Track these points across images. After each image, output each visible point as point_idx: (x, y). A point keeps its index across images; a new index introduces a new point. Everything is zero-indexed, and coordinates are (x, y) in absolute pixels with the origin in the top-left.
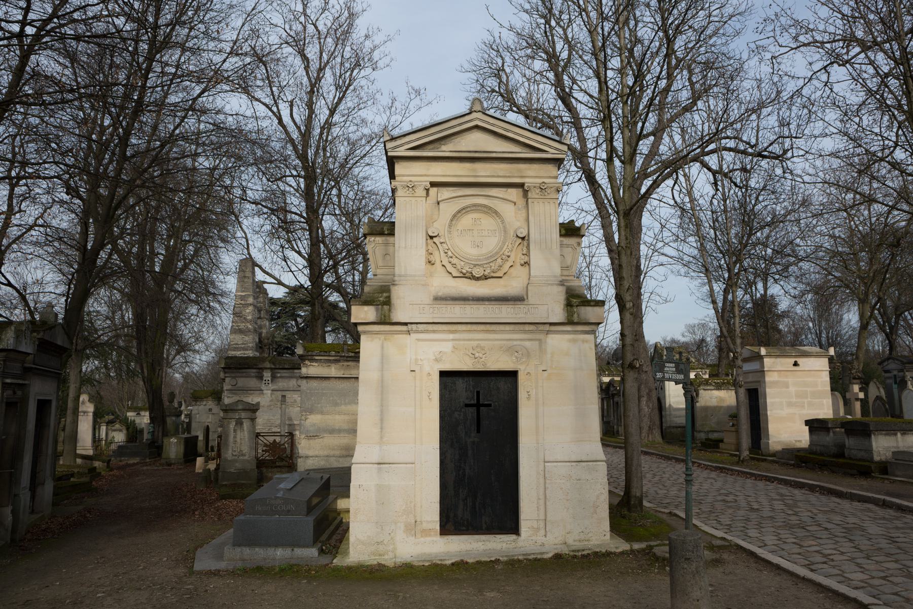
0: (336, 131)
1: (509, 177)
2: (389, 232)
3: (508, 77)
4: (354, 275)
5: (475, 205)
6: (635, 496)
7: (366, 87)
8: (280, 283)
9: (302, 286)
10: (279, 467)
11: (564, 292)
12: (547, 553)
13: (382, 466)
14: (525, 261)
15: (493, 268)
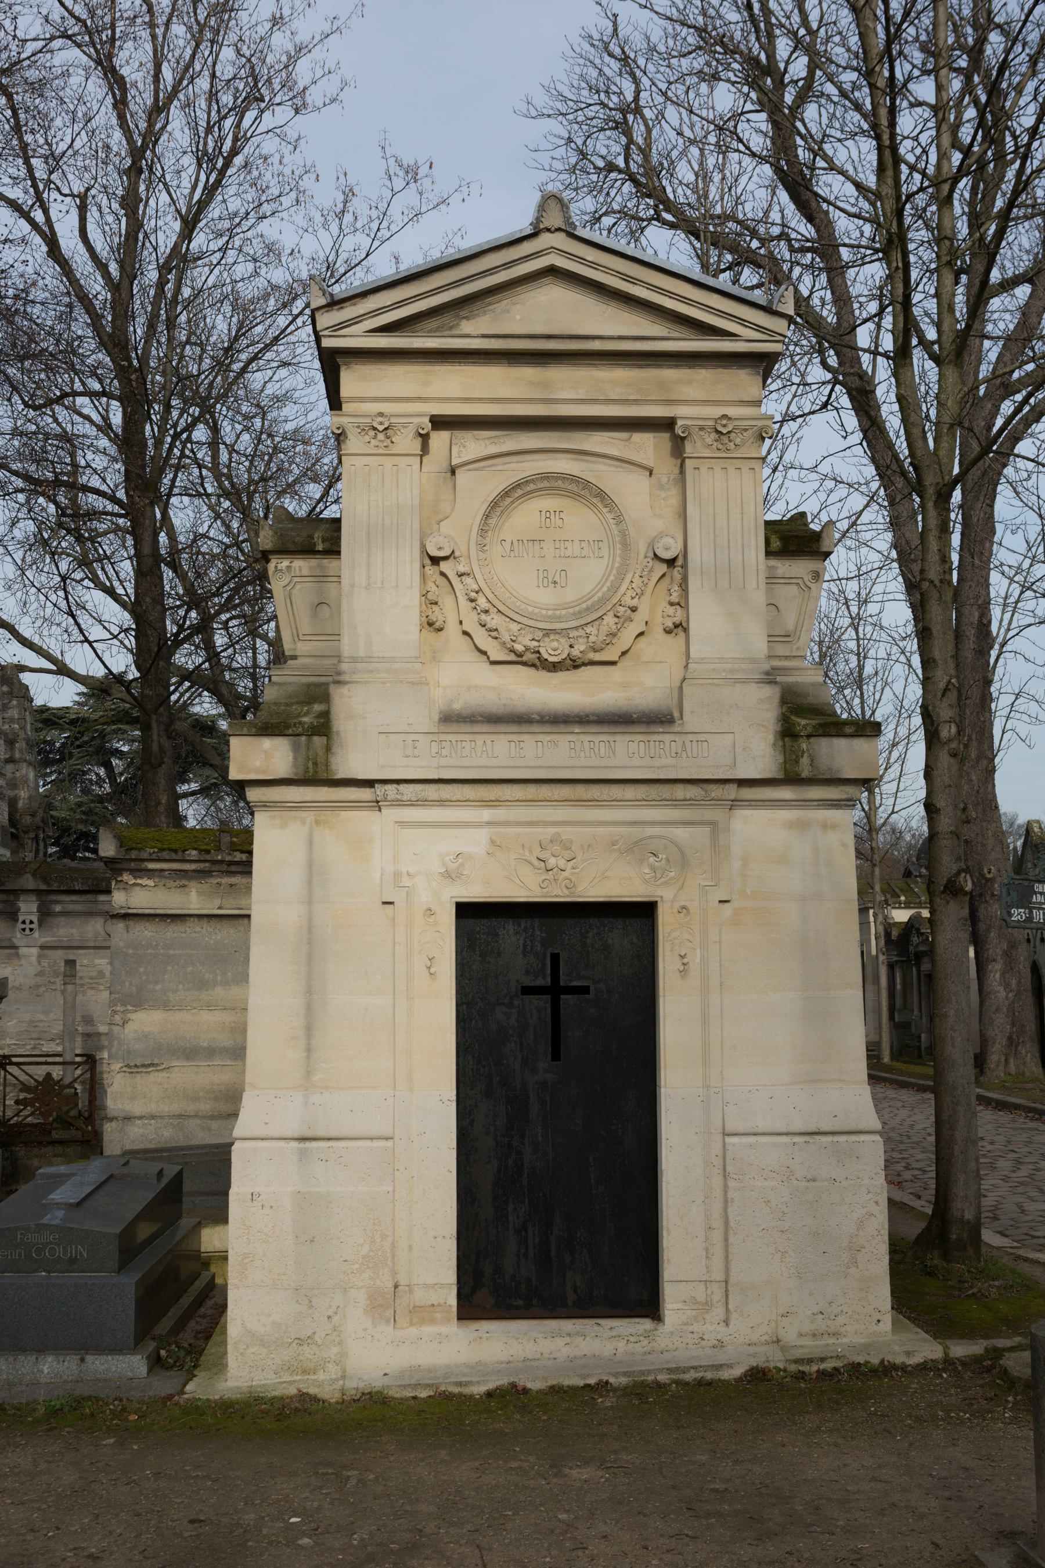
0: (199, 275)
1: (636, 402)
2: (327, 545)
3: (649, 131)
4: (254, 649)
5: (546, 477)
6: (962, 1220)
7: (277, 157)
8: (63, 670)
9: (119, 679)
10: (60, 1142)
11: (776, 700)
12: (730, 1366)
13: (308, 1144)
14: (677, 620)
15: (592, 638)
